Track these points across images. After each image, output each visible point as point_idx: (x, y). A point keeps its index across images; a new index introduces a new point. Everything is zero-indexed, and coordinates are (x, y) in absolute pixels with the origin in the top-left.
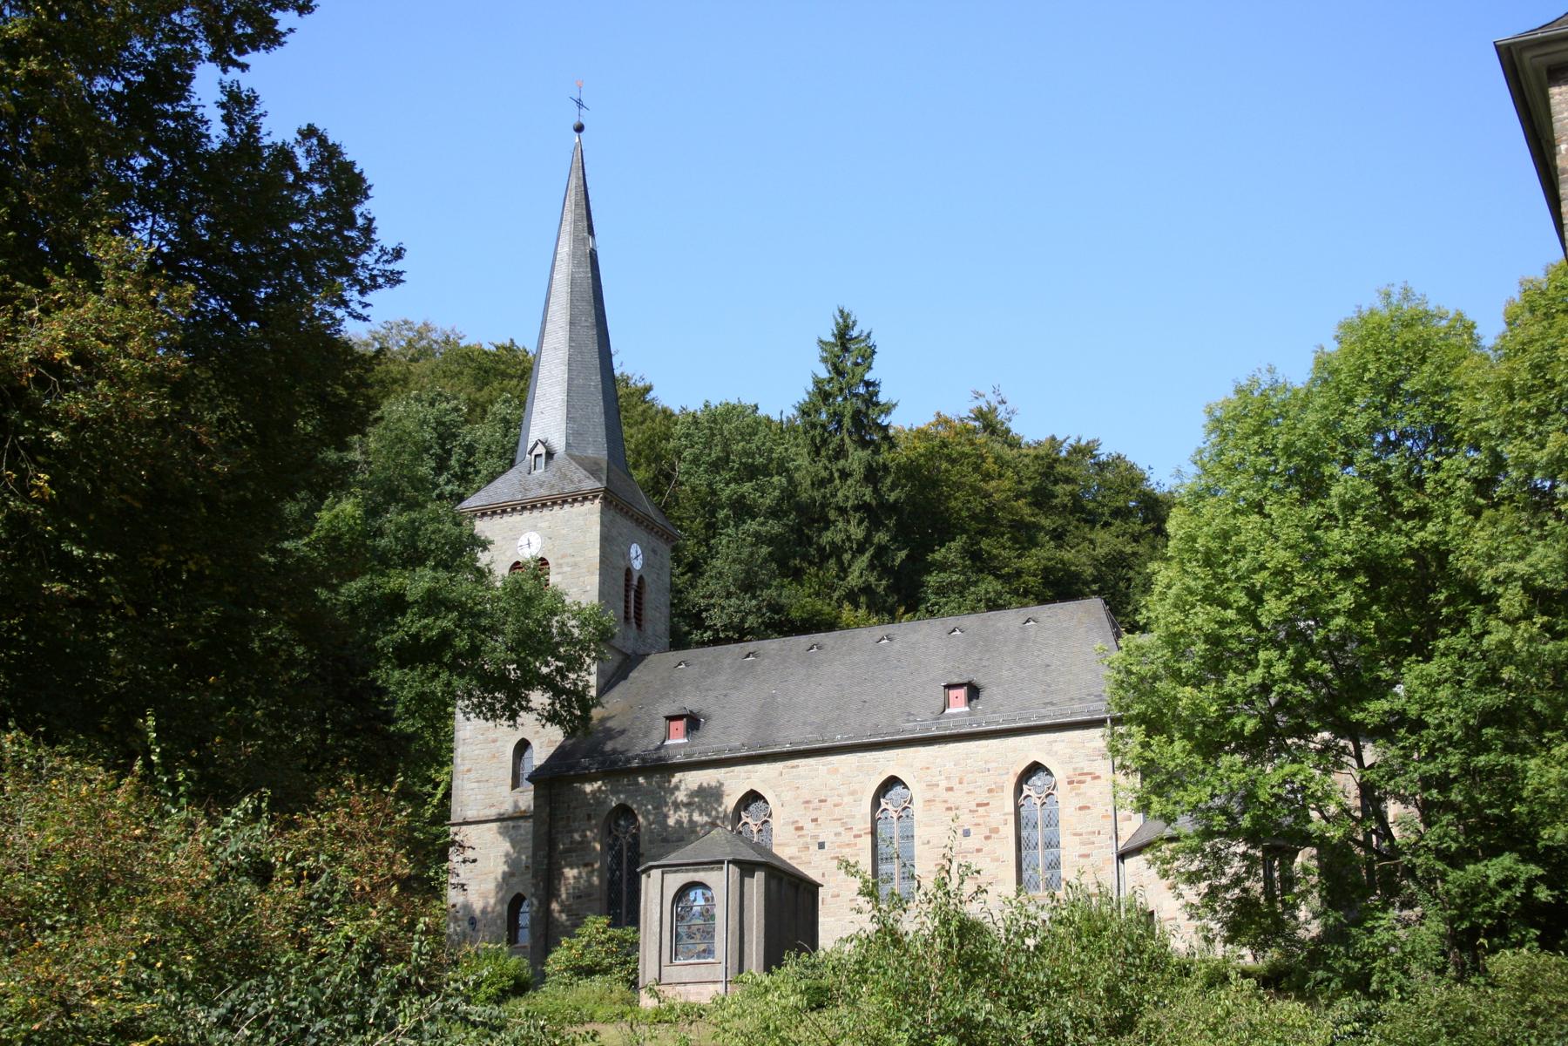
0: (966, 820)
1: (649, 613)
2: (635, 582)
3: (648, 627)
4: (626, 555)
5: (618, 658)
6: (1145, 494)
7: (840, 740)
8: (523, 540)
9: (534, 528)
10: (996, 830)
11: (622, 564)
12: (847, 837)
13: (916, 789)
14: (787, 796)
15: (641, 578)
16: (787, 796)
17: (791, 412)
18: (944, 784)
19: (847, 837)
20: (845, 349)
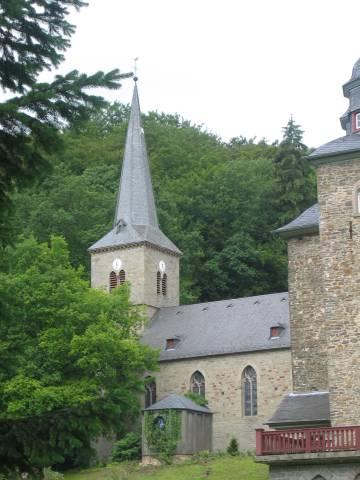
0: (276, 383)
1: (169, 289)
2: (162, 276)
3: (169, 295)
4: (157, 266)
5: (154, 311)
6: (84, 375)
7: (218, 350)
8: (114, 264)
9: (119, 257)
10: (287, 387)
11: (156, 271)
12: (232, 390)
13: (258, 372)
14: (210, 373)
15: (165, 275)
16: (210, 373)
17: (348, 100)
18: (268, 369)
19: (232, 390)
20: (188, 223)
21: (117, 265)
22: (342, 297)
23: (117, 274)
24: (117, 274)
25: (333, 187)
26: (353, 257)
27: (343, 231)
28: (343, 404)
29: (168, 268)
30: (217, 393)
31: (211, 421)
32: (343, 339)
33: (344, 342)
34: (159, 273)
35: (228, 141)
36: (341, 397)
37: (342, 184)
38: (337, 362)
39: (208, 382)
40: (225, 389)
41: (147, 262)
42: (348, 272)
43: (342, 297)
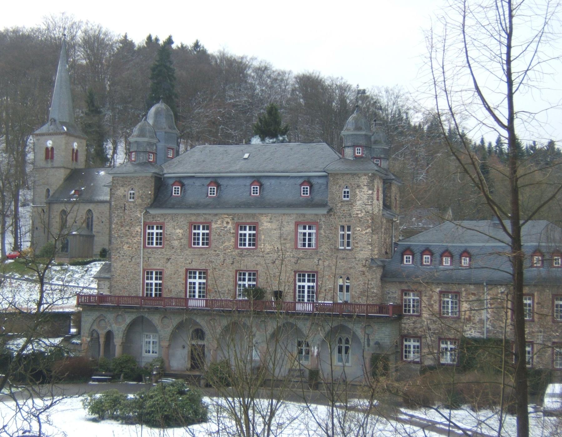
9: (51, 140)
11: (72, 148)
21: (49, 144)
22: (119, 236)
23: (50, 149)
24: (50, 149)
25: (118, 187)
26: (125, 219)
27: (121, 207)
28: (117, 283)
29: (78, 146)
30: (99, 222)
31: (93, 239)
32: (118, 255)
33: (119, 256)
34: (73, 150)
35: (130, 40)
36: (115, 280)
37: (122, 186)
38: (115, 264)
39: (95, 215)
40: (103, 220)
41: (67, 143)
42: (122, 226)
43: (119, 236)
